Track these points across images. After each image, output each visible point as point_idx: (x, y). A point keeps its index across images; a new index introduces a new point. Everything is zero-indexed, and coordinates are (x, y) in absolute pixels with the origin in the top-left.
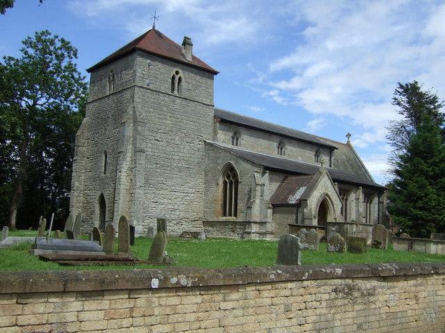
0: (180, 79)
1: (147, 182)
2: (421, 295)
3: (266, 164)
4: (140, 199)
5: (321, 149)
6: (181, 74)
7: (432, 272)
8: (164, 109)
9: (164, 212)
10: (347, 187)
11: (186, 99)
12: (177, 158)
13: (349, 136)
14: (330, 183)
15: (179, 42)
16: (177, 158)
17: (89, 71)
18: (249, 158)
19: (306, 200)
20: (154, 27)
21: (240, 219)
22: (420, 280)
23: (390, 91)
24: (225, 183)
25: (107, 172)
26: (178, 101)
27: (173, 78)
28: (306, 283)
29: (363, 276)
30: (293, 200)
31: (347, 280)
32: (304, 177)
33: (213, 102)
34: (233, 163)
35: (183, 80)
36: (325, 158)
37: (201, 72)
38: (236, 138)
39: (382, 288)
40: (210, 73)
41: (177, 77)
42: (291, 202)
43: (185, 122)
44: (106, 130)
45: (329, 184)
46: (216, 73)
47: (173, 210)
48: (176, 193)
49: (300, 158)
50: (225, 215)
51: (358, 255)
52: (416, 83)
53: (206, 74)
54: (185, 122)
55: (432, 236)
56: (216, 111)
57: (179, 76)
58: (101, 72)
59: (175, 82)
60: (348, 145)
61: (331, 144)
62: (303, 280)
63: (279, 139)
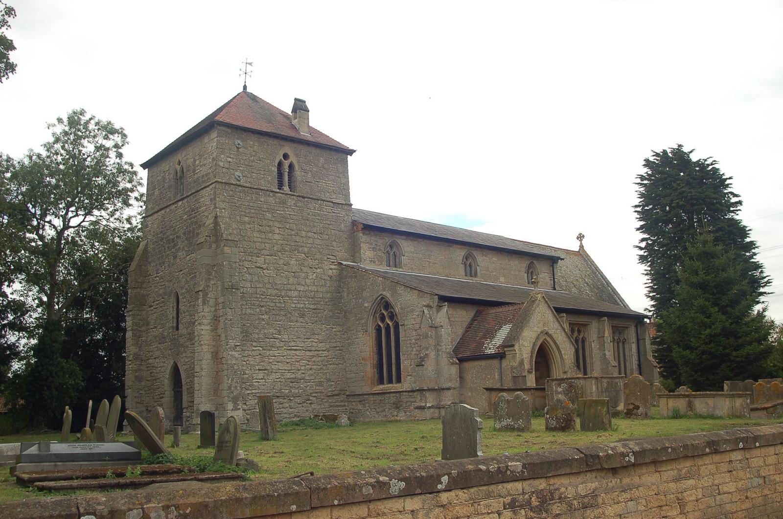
0: (291, 166)
1: (246, 335)
2: (690, 496)
3: (441, 293)
4: (236, 367)
5: (535, 262)
7: (708, 450)
8: (269, 215)
9: (278, 386)
10: (581, 319)
11: (304, 197)
12: (296, 293)
13: (581, 237)
15: (288, 108)
16: (296, 293)
17: (144, 166)
18: (414, 284)
19: (513, 346)
20: (245, 87)
21: (406, 385)
22: (685, 466)
24: (378, 330)
25: (180, 326)
26: (291, 202)
27: (280, 164)
28: (444, 497)
29: (568, 471)
31: (536, 482)
32: (511, 308)
34: (387, 294)
35: (297, 167)
39: (608, 491)
41: (286, 164)
42: (489, 352)
43: (304, 234)
44: (175, 258)
45: (549, 316)
46: (351, 152)
47: (295, 380)
48: (298, 353)
49: (502, 279)
50: (381, 381)
54: (304, 234)
55: (726, 387)
57: (289, 161)
58: (164, 166)
60: (581, 254)
61: (556, 255)
62: (439, 492)
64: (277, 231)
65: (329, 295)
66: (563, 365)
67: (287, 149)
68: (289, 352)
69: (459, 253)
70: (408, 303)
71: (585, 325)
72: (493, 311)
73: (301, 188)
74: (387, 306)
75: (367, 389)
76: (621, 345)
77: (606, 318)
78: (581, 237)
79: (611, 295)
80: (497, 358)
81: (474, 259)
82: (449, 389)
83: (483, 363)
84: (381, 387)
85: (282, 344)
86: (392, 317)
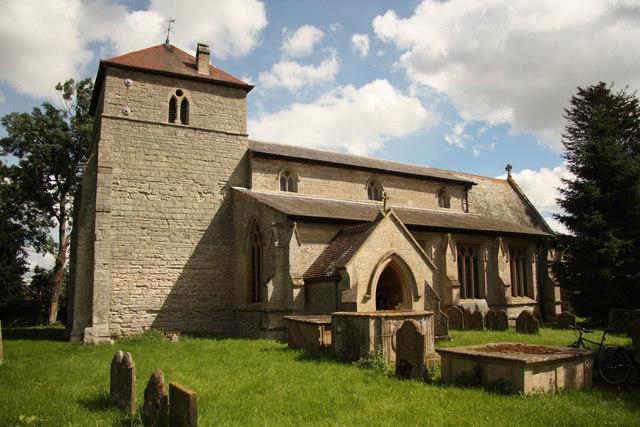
0: (185, 103)
6: (186, 93)
10: (472, 239)
12: (183, 216)
13: (509, 168)
14: (402, 237)
15: (194, 54)
16: (183, 216)
26: (181, 133)
27: (173, 101)
33: (245, 131)
36: (455, 202)
37: (223, 90)
38: (289, 184)
40: (241, 90)
41: (179, 100)
46: (248, 88)
49: (410, 202)
51: (498, 333)
52: (603, 84)
53: (233, 91)
59: (178, 112)
63: (367, 176)
64: (165, 159)
73: (193, 121)
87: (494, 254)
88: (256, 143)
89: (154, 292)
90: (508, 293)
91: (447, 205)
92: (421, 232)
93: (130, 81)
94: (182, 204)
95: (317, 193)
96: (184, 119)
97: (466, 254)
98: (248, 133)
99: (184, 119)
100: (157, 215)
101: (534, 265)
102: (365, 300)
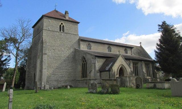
0: (63, 26)
10: (136, 62)
12: (63, 56)
13: (140, 43)
15: (64, 14)
23: (157, 28)
26: (63, 34)
27: (60, 26)
30: (107, 69)
35: (65, 26)
37: (72, 23)
38: (89, 47)
41: (62, 25)
42: (107, 70)
43: (66, 42)
46: (78, 23)
50: (83, 77)
53: (75, 24)
54: (66, 42)
56: (79, 37)
59: (62, 28)
61: (132, 46)
64: (59, 41)
65: (72, 56)
66: (127, 73)
67: (62, 22)
68: (61, 70)
69: (107, 46)
70: (88, 57)
71: (137, 63)
72: (109, 59)
73: (65, 31)
74: (85, 59)
75: (80, 79)
76: (148, 68)
77: (143, 61)
78: (140, 43)
79: (149, 56)
80: (108, 71)
81: (90, 44)
82: (97, 79)
83: (106, 72)
84: (83, 78)
85: (59, 68)
86: (86, 61)
87: (142, 65)
88: (81, 37)
89: (57, 76)
90: (146, 75)
91: (127, 53)
92: (127, 59)
93: (50, 20)
94: (63, 53)
95: (96, 49)
96: (63, 31)
97: (135, 65)
98: (79, 34)
99: (63, 31)
100: (57, 55)
101: (151, 68)
102: (117, 75)
